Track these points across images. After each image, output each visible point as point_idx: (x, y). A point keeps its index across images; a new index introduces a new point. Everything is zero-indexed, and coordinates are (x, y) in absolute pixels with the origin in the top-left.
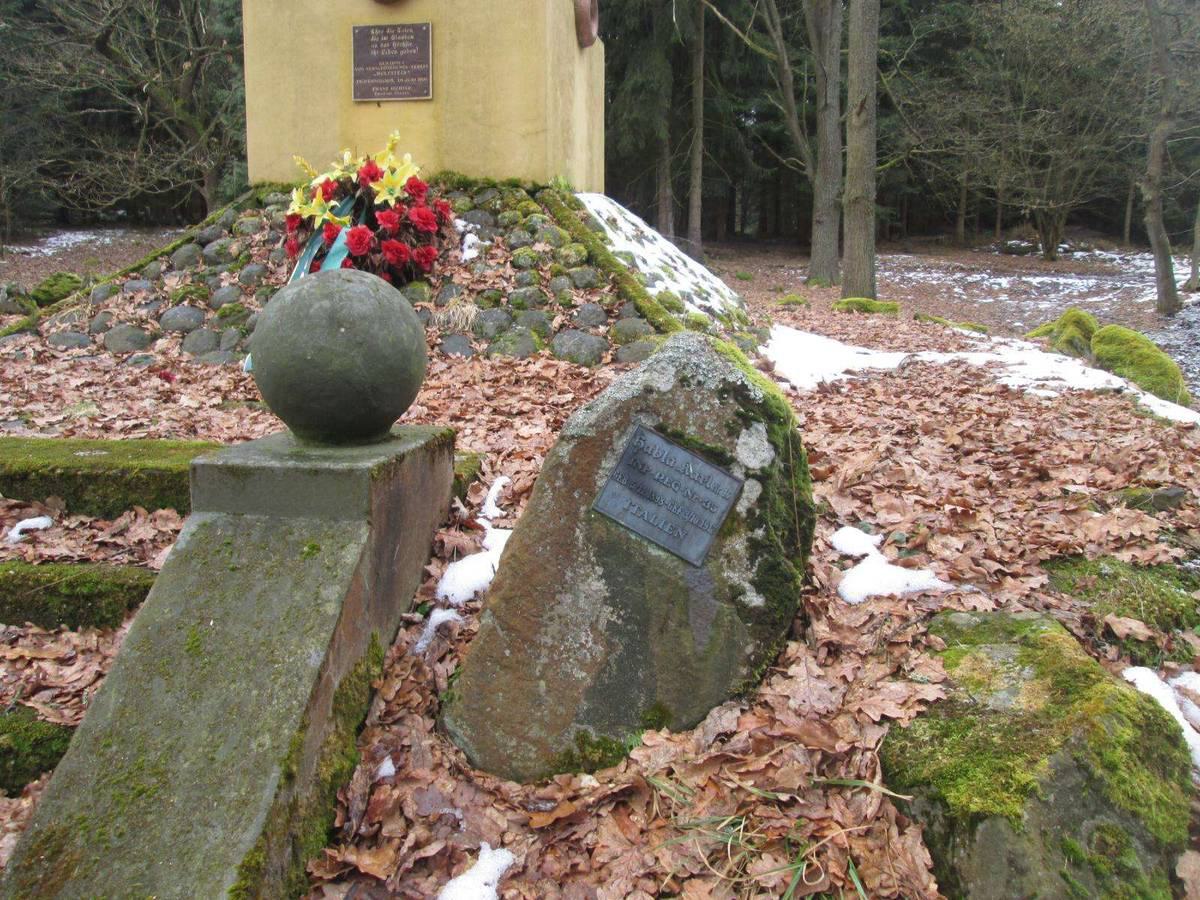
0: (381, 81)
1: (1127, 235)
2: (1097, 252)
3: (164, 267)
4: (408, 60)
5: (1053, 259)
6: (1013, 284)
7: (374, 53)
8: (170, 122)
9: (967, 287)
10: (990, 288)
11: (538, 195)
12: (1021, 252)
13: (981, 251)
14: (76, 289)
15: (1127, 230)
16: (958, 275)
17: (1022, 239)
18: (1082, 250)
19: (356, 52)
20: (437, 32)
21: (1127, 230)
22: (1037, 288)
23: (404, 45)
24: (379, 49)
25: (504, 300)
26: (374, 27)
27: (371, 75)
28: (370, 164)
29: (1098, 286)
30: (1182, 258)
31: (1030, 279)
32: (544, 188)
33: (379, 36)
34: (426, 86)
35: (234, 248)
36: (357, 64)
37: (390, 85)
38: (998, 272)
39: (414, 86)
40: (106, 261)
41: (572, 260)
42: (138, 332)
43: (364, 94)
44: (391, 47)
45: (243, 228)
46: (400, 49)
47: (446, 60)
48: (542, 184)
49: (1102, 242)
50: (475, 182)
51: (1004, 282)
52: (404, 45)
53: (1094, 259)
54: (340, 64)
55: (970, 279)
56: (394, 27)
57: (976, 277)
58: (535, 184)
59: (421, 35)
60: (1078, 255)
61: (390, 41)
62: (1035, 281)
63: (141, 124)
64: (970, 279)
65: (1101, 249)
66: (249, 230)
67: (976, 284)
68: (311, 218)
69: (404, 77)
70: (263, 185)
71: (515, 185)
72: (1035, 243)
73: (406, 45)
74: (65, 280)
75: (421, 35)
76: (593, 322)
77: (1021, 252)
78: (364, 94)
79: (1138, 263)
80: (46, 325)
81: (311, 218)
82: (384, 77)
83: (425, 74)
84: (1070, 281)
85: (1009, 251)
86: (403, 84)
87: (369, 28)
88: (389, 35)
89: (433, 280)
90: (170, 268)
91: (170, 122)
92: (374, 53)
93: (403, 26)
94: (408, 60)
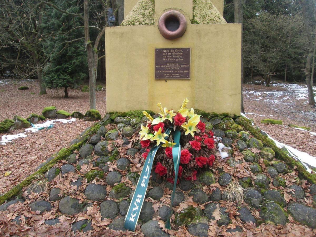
0: (168, 71)
1: (285, 79)
2: (279, 84)
3: (77, 157)
4: (180, 63)
5: (269, 86)
6: (261, 94)
7: (165, 60)
8: (27, 51)
9: (250, 95)
10: (256, 95)
11: (237, 120)
12: (259, 84)
13: (249, 84)
14: (12, 125)
15: (285, 78)
16: (247, 92)
17: (259, 80)
18: (275, 83)
19: (156, 59)
20: (193, 52)
21: (285, 78)
22: (268, 95)
23: (178, 57)
24: (167, 58)
25: (253, 183)
26: (165, 49)
27: (162, 69)
28: (179, 115)
29: (284, 94)
30: (301, 86)
31: (266, 93)
32: (239, 117)
33: (167, 53)
34: (188, 74)
35: (109, 148)
36: (157, 64)
37: (171, 73)
38: (256, 90)
39: (182, 74)
40: (7, 90)
41: (270, 157)
42: (76, 202)
43: (159, 76)
44: (172, 58)
45: (110, 136)
46: (176, 58)
47: (196, 64)
48: (238, 115)
49: (279, 81)
50: (209, 114)
51: (259, 93)
52: (178, 57)
53: (279, 86)
54: (149, 64)
55: (250, 93)
56: (174, 49)
57: (251, 92)
58: (235, 116)
59: (186, 53)
60: (274, 85)
61: (172, 55)
62: (268, 93)
63: (18, 51)
64: (250, 93)
65: (280, 83)
66: (114, 137)
67: (252, 94)
68: (155, 141)
69: (178, 70)
70: (113, 113)
71: (226, 116)
72: (263, 81)
73: (179, 58)
74: (8, 122)
75: (186, 53)
76: (302, 197)
77: (259, 84)
78: (159, 76)
79: (290, 87)
80: (26, 193)
81: (155, 141)
82: (169, 70)
83: (188, 69)
84: (276, 93)
85: (256, 84)
86: (177, 73)
87: (163, 49)
88: (172, 53)
89: (214, 170)
90: (80, 157)
91: (27, 51)
92: (165, 60)
93: (178, 49)
94: (180, 63)
